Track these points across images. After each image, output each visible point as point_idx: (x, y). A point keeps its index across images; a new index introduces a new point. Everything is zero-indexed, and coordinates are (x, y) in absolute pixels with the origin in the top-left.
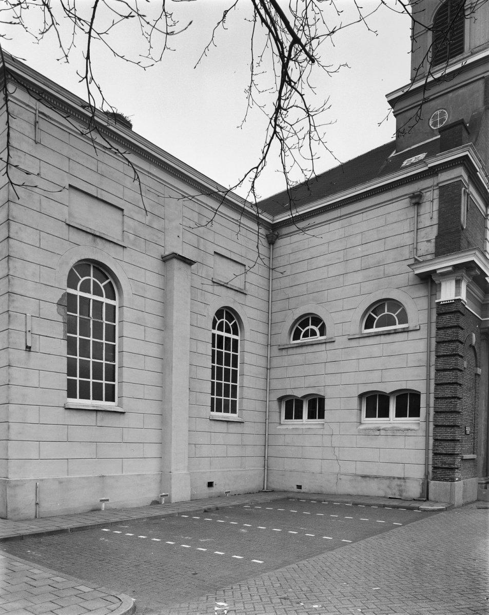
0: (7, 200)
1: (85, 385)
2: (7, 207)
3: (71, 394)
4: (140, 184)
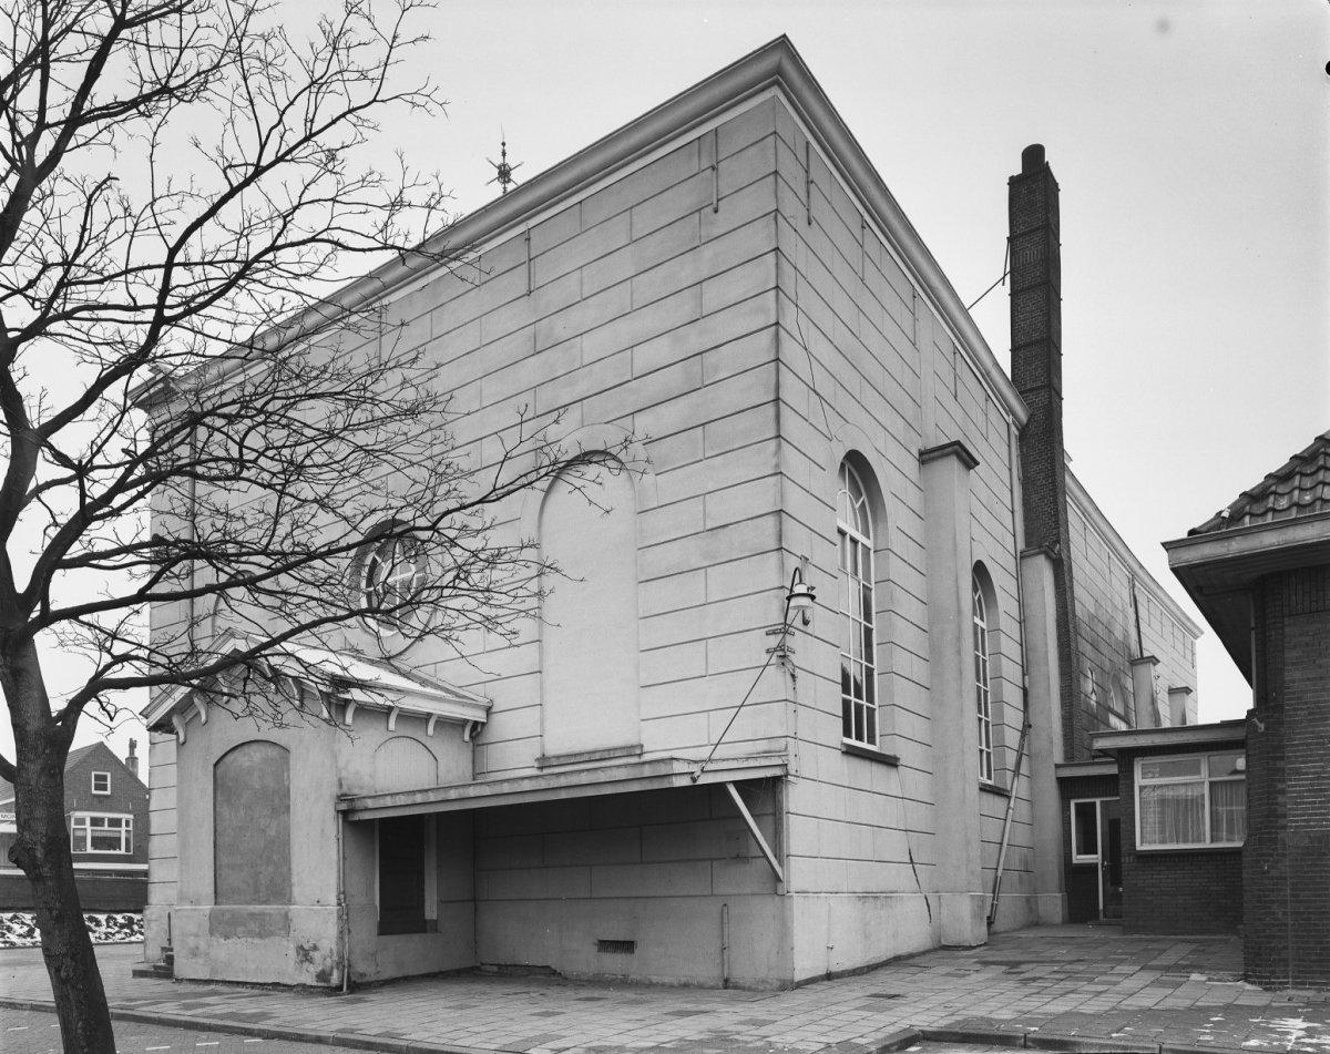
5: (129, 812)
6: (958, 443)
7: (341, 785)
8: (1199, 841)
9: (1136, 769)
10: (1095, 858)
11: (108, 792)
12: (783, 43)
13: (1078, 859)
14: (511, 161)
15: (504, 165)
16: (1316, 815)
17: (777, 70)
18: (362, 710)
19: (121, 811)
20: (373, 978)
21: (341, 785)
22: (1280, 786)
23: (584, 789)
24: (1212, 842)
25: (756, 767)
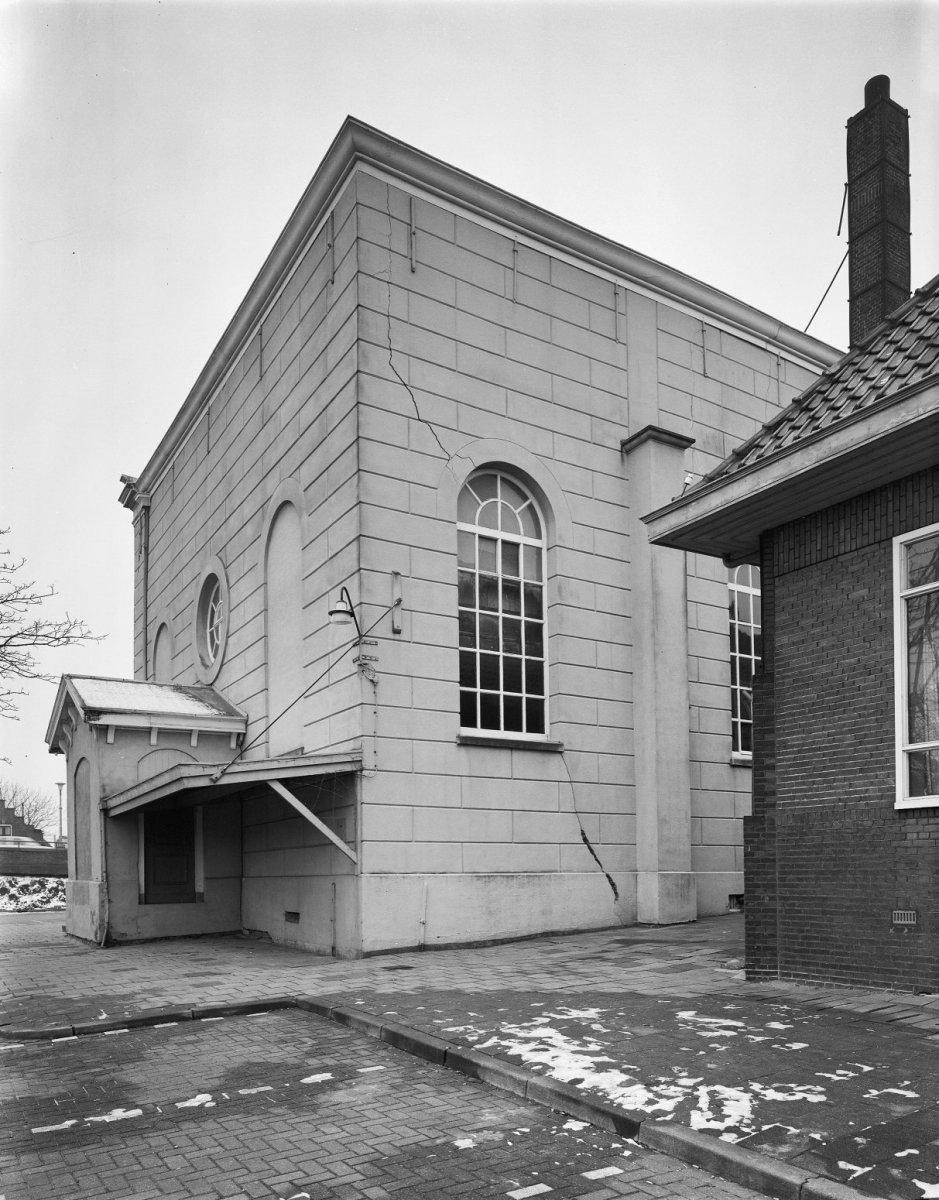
0: (356, 370)
1: (490, 703)
2: (355, 451)
3: (467, 720)
4: (591, 851)
6: (650, 428)
7: (104, 790)
12: (351, 124)
17: (359, 147)
18: (121, 731)
20: (135, 937)
21: (104, 790)
22: (768, 761)
23: (138, 800)
25: (293, 767)
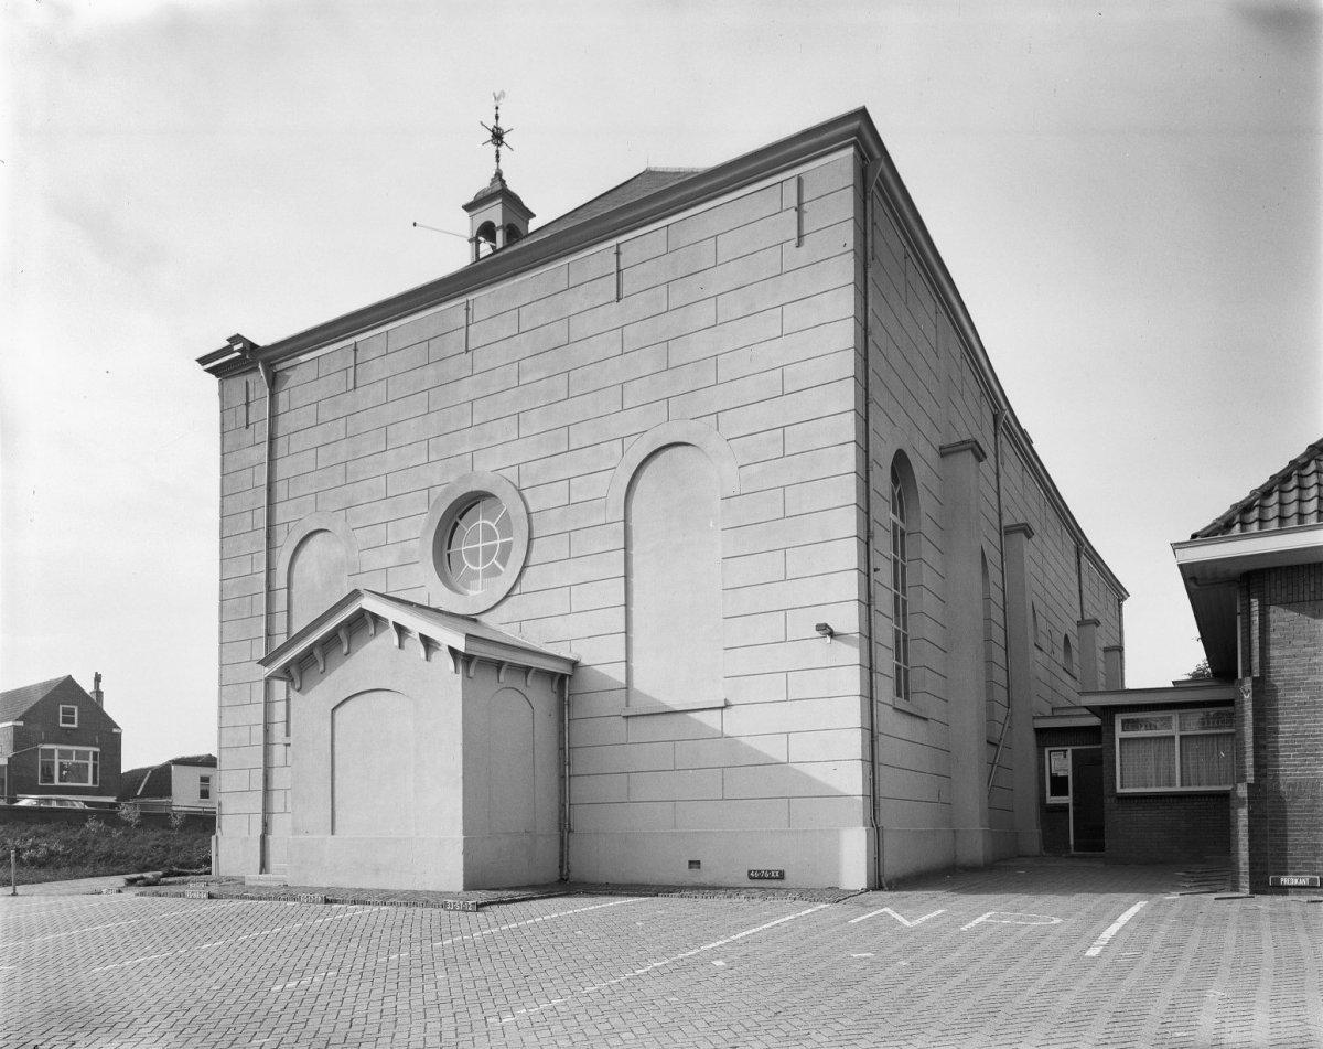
5: (95, 745)
8: (1170, 785)
9: (1116, 722)
10: (1068, 800)
11: (75, 726)
13: (1051, 800)
14: (501, 124)
15: (498, 129)
16: (1291, 765)
19: (88, 745)
24: (1182, 785)
